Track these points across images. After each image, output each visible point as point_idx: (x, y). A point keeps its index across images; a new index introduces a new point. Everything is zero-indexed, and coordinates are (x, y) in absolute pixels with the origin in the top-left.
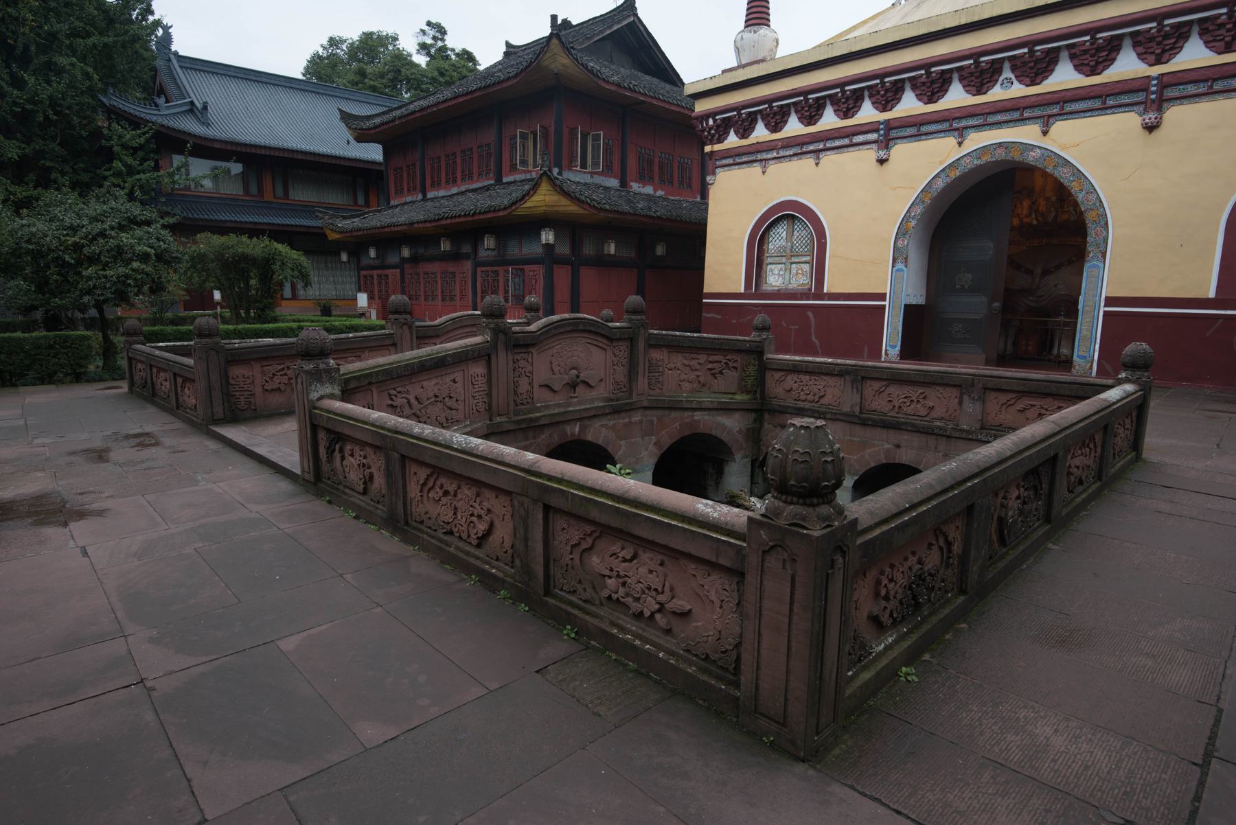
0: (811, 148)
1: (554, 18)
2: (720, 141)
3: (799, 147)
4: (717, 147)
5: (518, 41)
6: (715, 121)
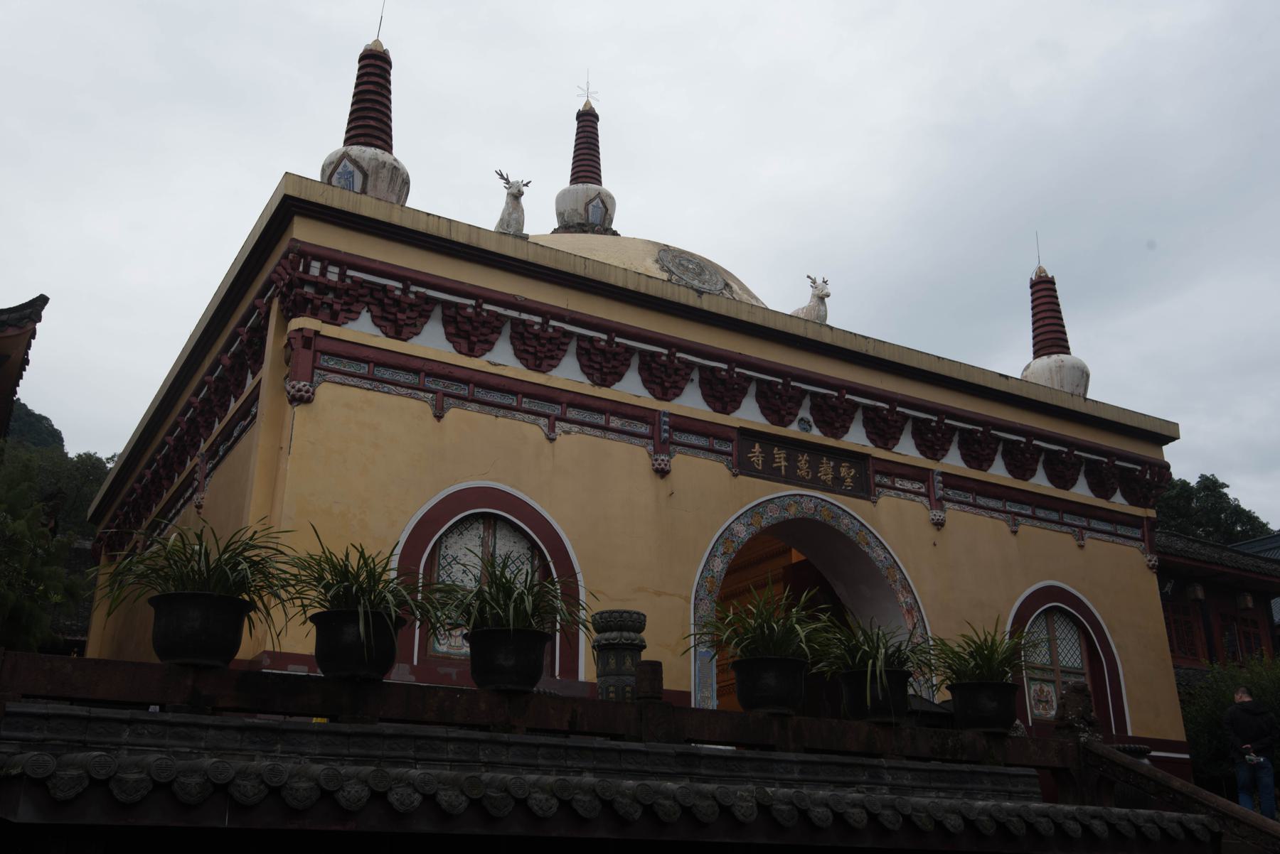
2: (334, 319)
4: (329, 330)
6: (342, 275)
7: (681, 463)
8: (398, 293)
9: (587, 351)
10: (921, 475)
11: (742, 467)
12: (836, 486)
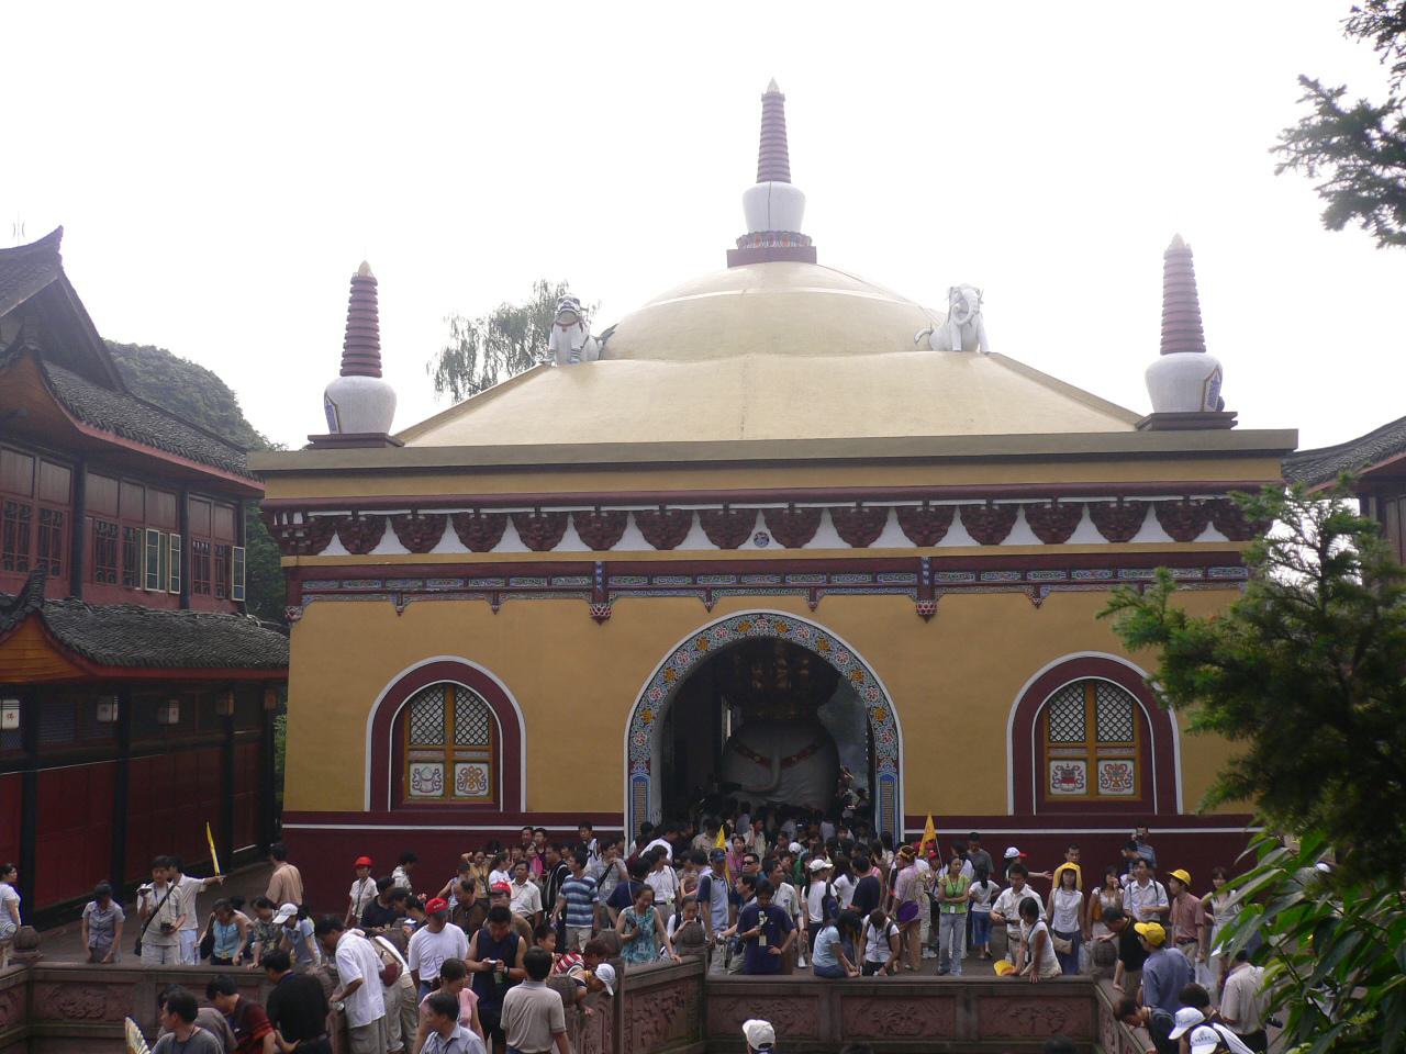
0: (483, 584)
1: (1380, 245)
2: (312, 551)
3: (461, 579)
4: (306, 560)
5: (81, 270)
6: (306, 518)
10: (586, 569)
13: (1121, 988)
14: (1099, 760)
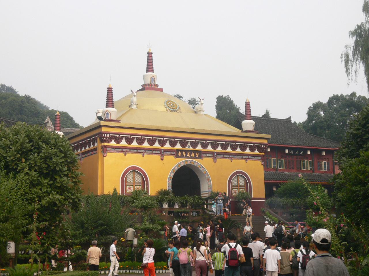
2: (109, 142)
6: (109, 135)
7: (219, 160)
8: (118, 136)
9: (202, 144)
10: (159, 150)
11: (177, 156)
12: (195, 157)
13: (337, 231)
14: (240, 189)
